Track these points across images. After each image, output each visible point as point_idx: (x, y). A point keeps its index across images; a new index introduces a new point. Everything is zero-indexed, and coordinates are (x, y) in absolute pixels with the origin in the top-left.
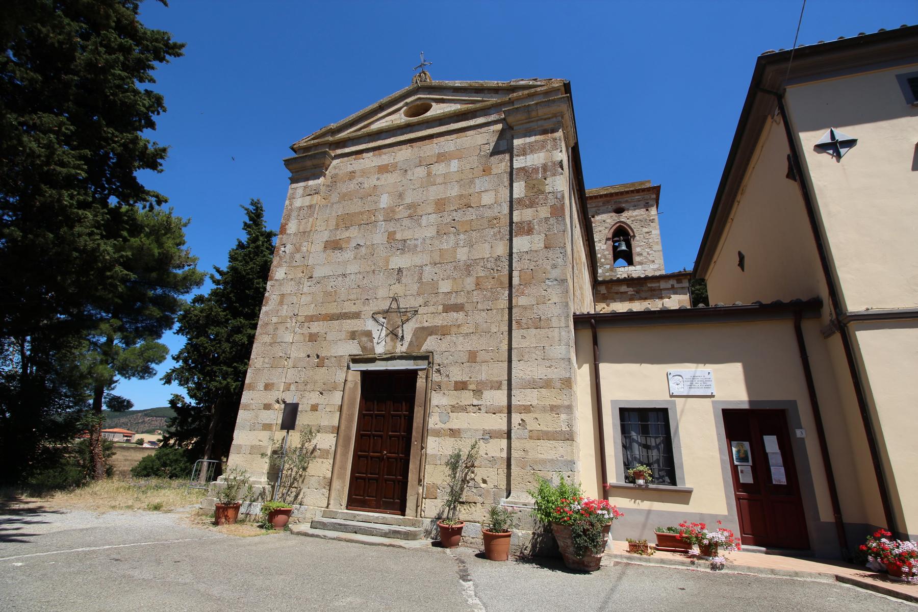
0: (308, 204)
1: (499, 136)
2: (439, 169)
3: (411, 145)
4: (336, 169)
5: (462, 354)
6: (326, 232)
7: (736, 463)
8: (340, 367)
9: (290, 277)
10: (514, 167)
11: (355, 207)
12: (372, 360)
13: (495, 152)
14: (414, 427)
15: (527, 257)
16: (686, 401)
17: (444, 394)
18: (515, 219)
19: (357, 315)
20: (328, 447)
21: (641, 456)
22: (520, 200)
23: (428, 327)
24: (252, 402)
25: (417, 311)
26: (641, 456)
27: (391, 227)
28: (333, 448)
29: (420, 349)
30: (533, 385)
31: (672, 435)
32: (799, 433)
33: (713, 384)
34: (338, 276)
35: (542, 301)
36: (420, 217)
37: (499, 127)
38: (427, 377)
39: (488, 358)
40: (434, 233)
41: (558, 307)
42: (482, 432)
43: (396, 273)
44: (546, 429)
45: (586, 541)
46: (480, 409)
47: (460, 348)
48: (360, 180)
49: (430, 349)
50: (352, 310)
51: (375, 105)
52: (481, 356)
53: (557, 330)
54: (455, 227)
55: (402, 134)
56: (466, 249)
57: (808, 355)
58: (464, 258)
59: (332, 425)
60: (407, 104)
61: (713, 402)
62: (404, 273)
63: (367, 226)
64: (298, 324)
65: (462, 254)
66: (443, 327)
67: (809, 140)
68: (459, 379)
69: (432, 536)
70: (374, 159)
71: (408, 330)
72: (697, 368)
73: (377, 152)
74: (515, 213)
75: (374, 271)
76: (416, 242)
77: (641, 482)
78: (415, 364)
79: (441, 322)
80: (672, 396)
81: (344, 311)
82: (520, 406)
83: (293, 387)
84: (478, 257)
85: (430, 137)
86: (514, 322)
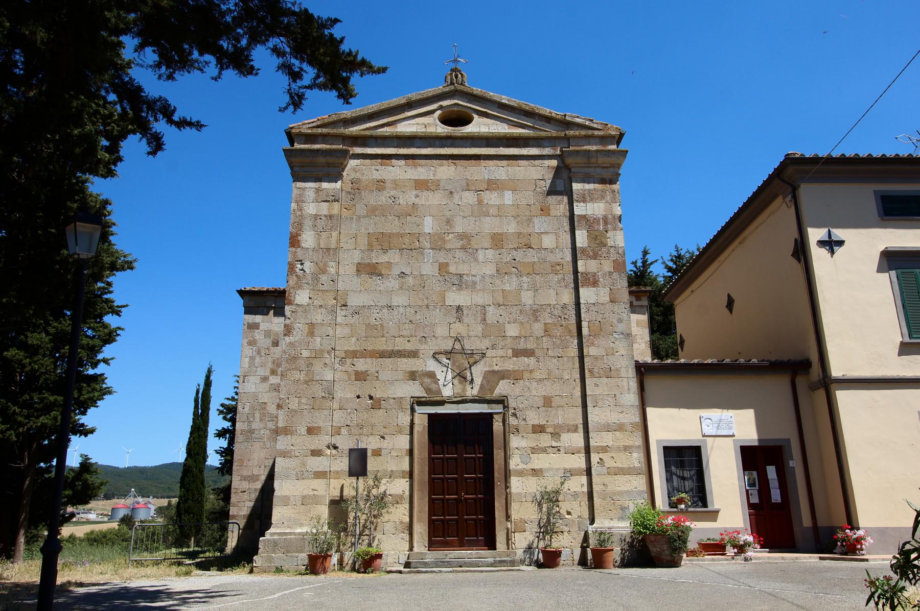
0: (325, 212)
1: (554, 174)
2: (492, 198)
3: (454, 161)
4: (356, 172)
5: (537, 399)
6: (357, 252)
7: (748, 488)
8: (402, 409)
9: (317, 303)
10: (575, 213)
11: (391, 226)
12: (441, 403)
13: (552, 192)
14: (495, 469)
15: (593, 308)
16: (714, 440)
17: (523, 436)
18: (580, 269)
19: (414, 354)
20: (401, 493)
21: (680, 486)
22: (583, 250)
23: (498, 371)
24: (292, 448)
25: (485, 354)
26: (680, 486)
27: (442, 257)
28: (407, 493)
29: (493, 393)
30: (608, 428)
31: (704, 468)
32: (792, 464)
33: (734, 425)
34: (383, 307)
35: (611, 352)
36: (475, 251)
37: (554, 163)
38: (504, 421)
39: (563, 404)
40: (494, 271)
41: (626, 359)
42: (563, 471)
43: (455, 311)
44: (621, 466)
45: (680, 543)
46: (559, 450)
47: (534, 393)
48: (392, 193)
49: (504, 393)
50: (407, 348)
51: (402, 100)
52: (556, 401)
53: (626, 379)
54: (517, 269)
55: (442, 146)
56: (530, 294)
57: (800, 404)
58: (530, 302)
59: (402, 469)
60: (441, 107)
61: (734, 440)
62: (465, 312)
63: (411, 252)
64: (337, 360)
65: (527, 298)
66: (514, 371)
67: (815, 235)
68: (536, 422)
69: (527, 563)
70: (409, 169)
71: (478, 372)
72: (722, 412)
73: (410, 161)
74: (580, 263)
75: (427, 306)
76: (474, 279)
77: (683, 506)
78: (489, 408)
79: (512, 366)
80: (704, 436)
81: (396, 348)
82: (598, 446)
83: (344, 431)
84: (544, 303)
85: (477, 157)
86: (586, 371)
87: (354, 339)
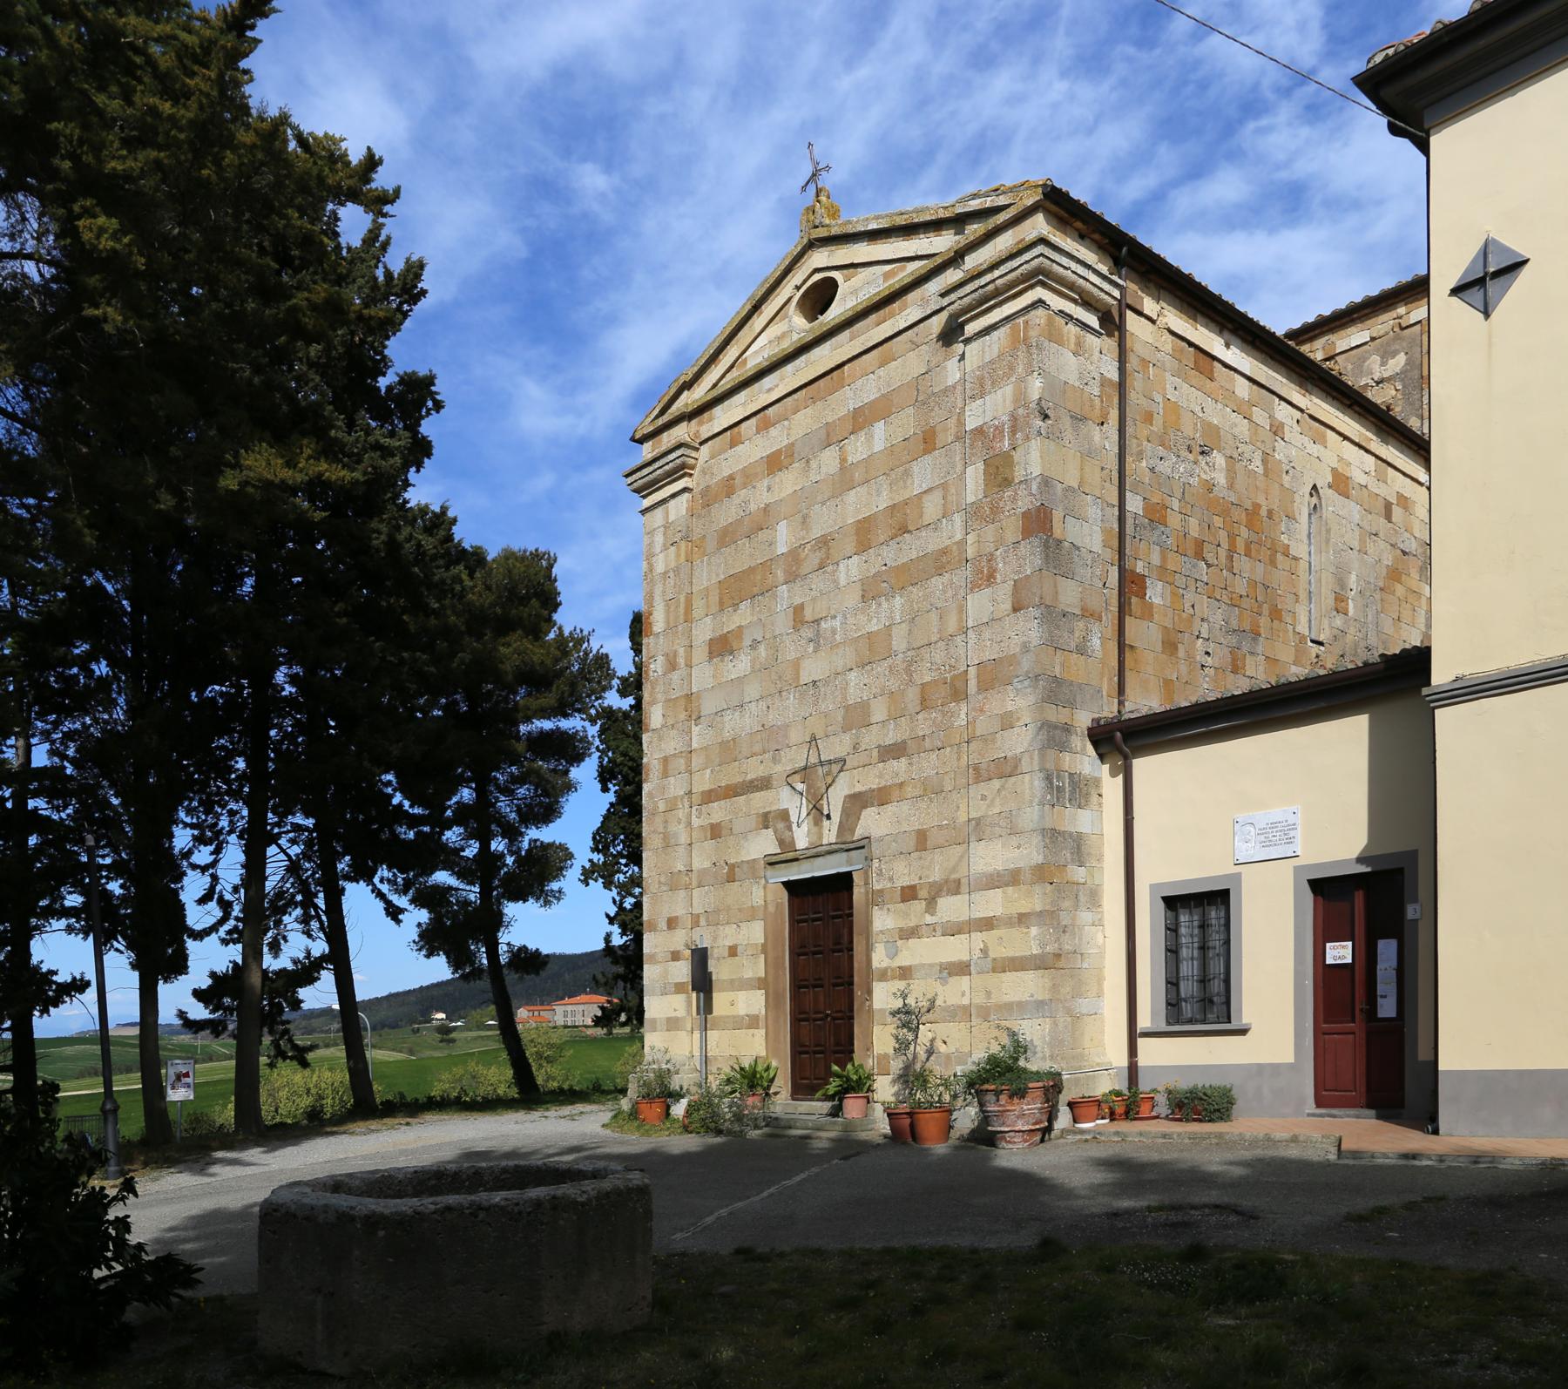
2: (857, 448)
71: (835, 802)
87: (708, 771)
